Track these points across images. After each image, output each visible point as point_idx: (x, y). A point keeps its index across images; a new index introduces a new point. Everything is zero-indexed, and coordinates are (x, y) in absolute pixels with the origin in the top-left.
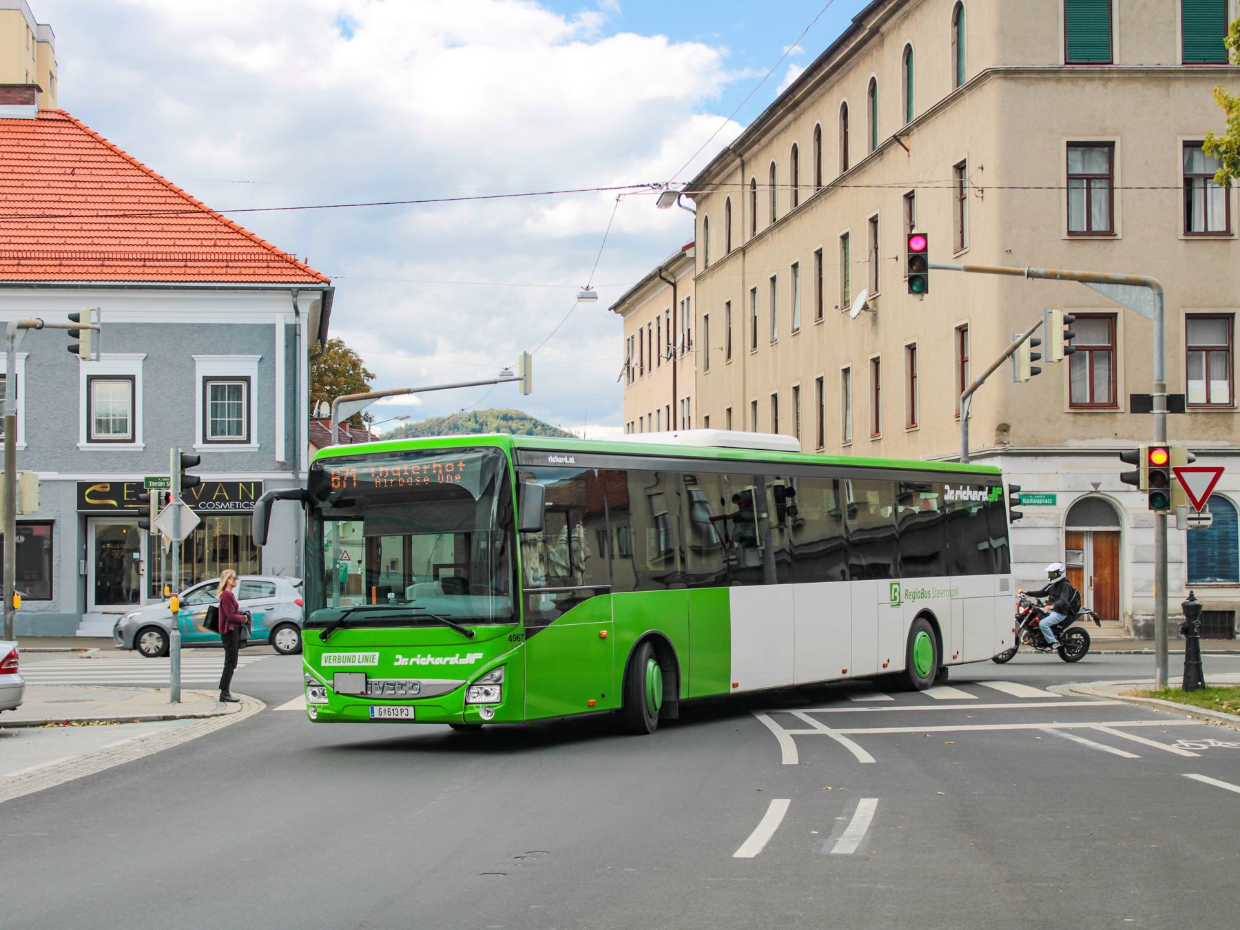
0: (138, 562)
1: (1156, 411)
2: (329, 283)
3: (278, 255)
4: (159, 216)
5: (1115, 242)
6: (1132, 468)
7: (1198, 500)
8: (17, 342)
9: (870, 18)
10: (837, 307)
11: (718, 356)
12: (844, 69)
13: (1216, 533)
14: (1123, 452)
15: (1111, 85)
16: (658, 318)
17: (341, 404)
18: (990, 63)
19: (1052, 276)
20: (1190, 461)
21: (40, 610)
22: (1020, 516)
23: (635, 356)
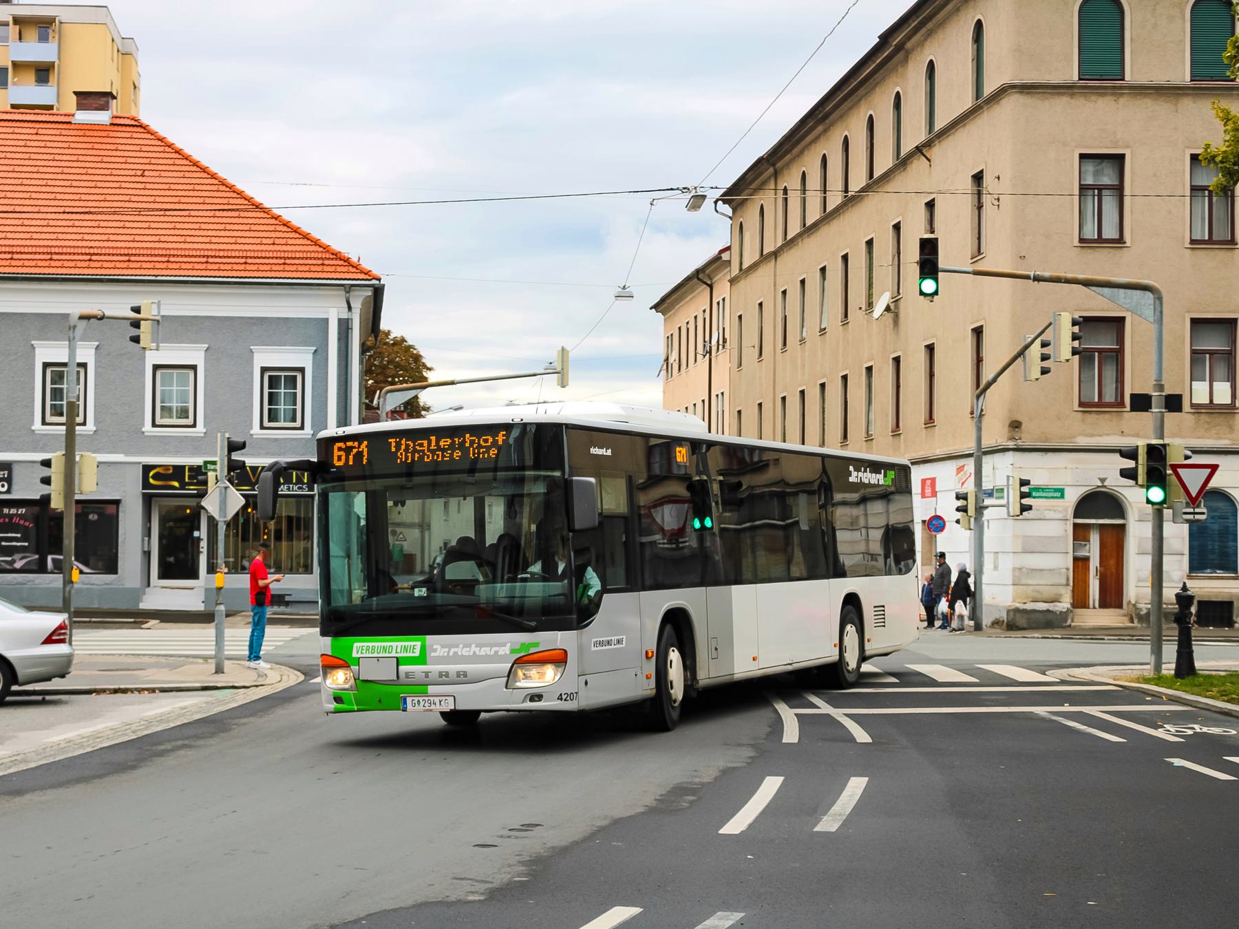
0: (199, 539)
1: (1154, 410)
2: (379, 280)
3: (333, 254)
4: (126, 213)
5: (1125, 249)
6: (1130, 464)
7: (1194, 495)
8: (79, 332)
9: (896, 35)
10: (860, 308)
11: (750, 354)
12: (870, 83)
13: (1216, 527)
14: (1122, 448)
15: (1122, 100)
16: (696, 317)
17: (389, 394)
18: (1006, 79)
19: (1057, 280)
20: (1187, 457)
21: (106, 584)
22: (1029, 508)
23: (674, 352)
